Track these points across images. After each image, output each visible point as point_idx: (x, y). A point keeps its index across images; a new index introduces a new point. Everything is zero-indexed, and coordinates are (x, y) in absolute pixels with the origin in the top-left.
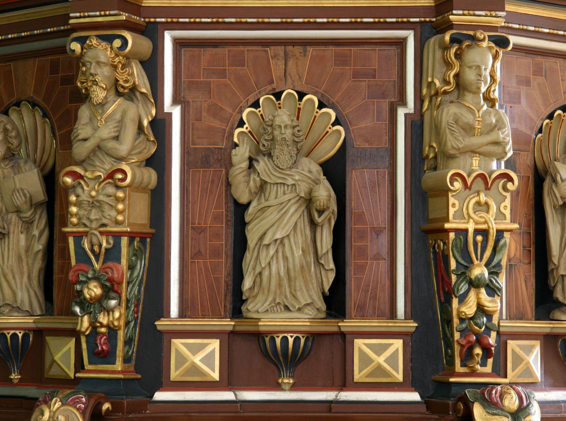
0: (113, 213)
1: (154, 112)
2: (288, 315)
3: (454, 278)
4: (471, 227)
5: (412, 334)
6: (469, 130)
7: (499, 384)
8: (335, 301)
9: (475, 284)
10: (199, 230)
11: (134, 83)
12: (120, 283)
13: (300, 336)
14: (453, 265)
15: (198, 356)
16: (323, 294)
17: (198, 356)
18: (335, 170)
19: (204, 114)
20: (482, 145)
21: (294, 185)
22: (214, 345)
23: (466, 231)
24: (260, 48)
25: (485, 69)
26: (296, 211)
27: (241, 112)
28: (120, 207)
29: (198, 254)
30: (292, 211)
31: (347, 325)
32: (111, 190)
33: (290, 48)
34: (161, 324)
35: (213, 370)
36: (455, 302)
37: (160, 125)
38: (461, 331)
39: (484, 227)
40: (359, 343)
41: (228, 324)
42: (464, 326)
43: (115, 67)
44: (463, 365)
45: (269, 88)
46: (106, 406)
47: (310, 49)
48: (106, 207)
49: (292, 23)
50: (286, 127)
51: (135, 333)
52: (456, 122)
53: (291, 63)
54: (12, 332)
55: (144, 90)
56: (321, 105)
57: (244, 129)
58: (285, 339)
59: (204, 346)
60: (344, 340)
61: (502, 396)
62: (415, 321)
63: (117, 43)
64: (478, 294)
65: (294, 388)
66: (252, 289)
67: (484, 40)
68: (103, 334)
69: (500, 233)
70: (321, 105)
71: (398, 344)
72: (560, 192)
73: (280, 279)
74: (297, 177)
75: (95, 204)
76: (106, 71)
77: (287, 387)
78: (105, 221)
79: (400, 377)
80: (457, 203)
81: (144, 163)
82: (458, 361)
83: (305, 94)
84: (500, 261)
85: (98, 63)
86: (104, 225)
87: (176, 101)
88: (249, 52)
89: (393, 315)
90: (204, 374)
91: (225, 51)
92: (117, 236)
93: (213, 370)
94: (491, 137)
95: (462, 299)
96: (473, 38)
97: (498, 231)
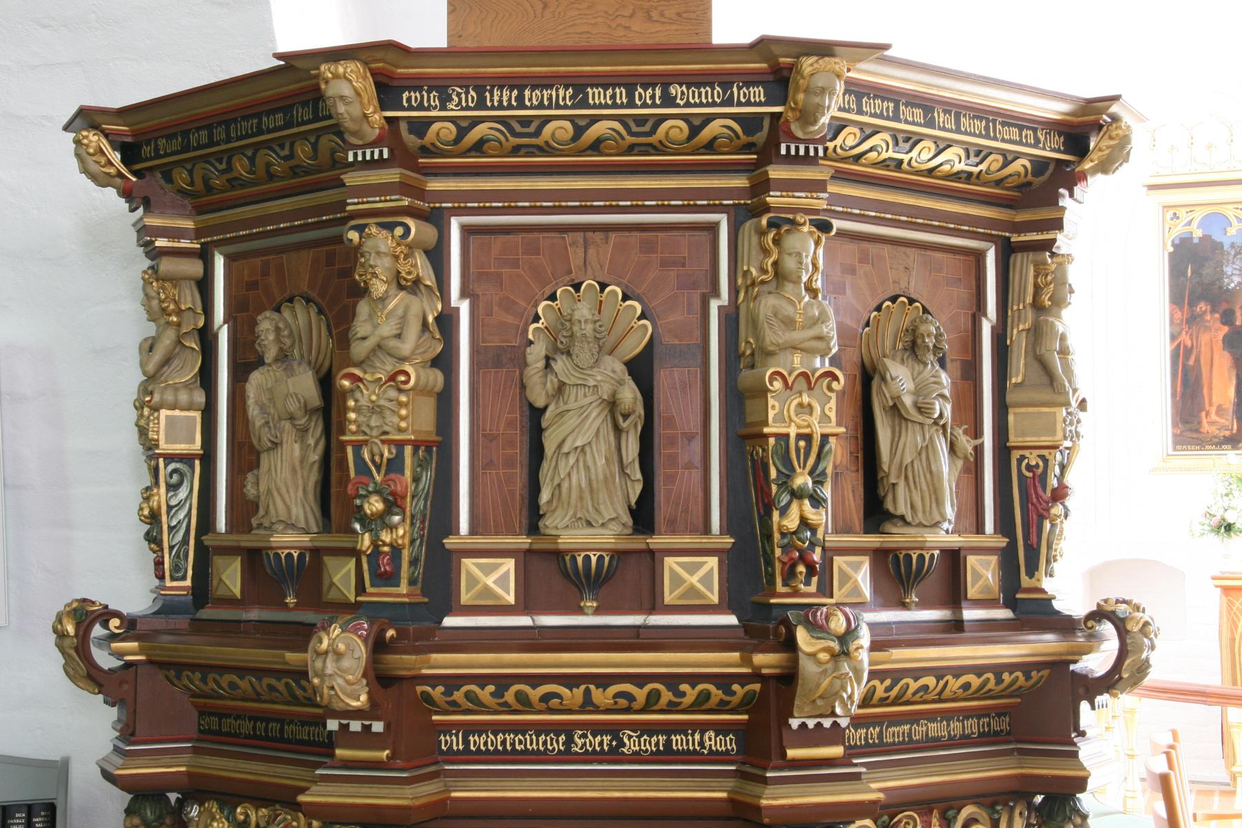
0: (396, 419)
1: (440, 307)
2: (590, 531)
3: (774, 488)
4: (793, 431)
5: (1002, 549)
6: (789, 323)
8: (643, 516)
9: (797, 495)
10: (491, 438)
12: (404, 497)
14: (773, 473)
15: (492, 577)
17: (492, 577)
18: (641, 369)
19: (495, 308)
21: (595, 386)
23: (787, 435)
26: (599, 415)
27: (536, 306)
28: (403, 412)
29: (489, 464)
31: (656, 541)
32: (392, 394)
33: (590, 234)
34: (450, 542)
35: (712, 593)
37: (447, 321)
39: (807, 431)
40: (670, 562)
41: (523, 541)
42: (786, 541)
43: (396, 258)
44: (785, 584)
45: (568, 278)
46: (391, 633)
48: (388, 413)
49: (618, 206)
50: (586, 321)
53: (591, 251)
55: (428, 283)
56: (626, 297)
57: (539, 325)
58: (587, 558)
59: (497, 566)
60: (653, 558)
61: (827, 619)
63: (399, 231)
64: (800, 506)
65: (598, 611)
66: (550, 502)
67: (804, 224)
68: (386, 553)
69: (825, 437)
70: (626, 297)
71: (712, 562)
74: (599, 378)
75: (376, 409)
76: (387, 261)
78: (386, 428)
80: (777, 404)
82: (779, 581)
83: (581, 283)
87: (464, 294)
89: (707, 530)
90: (497, 597)
92: (400, 445)
93: (712, 593)
95: (784, 511)
96: (793, 222)
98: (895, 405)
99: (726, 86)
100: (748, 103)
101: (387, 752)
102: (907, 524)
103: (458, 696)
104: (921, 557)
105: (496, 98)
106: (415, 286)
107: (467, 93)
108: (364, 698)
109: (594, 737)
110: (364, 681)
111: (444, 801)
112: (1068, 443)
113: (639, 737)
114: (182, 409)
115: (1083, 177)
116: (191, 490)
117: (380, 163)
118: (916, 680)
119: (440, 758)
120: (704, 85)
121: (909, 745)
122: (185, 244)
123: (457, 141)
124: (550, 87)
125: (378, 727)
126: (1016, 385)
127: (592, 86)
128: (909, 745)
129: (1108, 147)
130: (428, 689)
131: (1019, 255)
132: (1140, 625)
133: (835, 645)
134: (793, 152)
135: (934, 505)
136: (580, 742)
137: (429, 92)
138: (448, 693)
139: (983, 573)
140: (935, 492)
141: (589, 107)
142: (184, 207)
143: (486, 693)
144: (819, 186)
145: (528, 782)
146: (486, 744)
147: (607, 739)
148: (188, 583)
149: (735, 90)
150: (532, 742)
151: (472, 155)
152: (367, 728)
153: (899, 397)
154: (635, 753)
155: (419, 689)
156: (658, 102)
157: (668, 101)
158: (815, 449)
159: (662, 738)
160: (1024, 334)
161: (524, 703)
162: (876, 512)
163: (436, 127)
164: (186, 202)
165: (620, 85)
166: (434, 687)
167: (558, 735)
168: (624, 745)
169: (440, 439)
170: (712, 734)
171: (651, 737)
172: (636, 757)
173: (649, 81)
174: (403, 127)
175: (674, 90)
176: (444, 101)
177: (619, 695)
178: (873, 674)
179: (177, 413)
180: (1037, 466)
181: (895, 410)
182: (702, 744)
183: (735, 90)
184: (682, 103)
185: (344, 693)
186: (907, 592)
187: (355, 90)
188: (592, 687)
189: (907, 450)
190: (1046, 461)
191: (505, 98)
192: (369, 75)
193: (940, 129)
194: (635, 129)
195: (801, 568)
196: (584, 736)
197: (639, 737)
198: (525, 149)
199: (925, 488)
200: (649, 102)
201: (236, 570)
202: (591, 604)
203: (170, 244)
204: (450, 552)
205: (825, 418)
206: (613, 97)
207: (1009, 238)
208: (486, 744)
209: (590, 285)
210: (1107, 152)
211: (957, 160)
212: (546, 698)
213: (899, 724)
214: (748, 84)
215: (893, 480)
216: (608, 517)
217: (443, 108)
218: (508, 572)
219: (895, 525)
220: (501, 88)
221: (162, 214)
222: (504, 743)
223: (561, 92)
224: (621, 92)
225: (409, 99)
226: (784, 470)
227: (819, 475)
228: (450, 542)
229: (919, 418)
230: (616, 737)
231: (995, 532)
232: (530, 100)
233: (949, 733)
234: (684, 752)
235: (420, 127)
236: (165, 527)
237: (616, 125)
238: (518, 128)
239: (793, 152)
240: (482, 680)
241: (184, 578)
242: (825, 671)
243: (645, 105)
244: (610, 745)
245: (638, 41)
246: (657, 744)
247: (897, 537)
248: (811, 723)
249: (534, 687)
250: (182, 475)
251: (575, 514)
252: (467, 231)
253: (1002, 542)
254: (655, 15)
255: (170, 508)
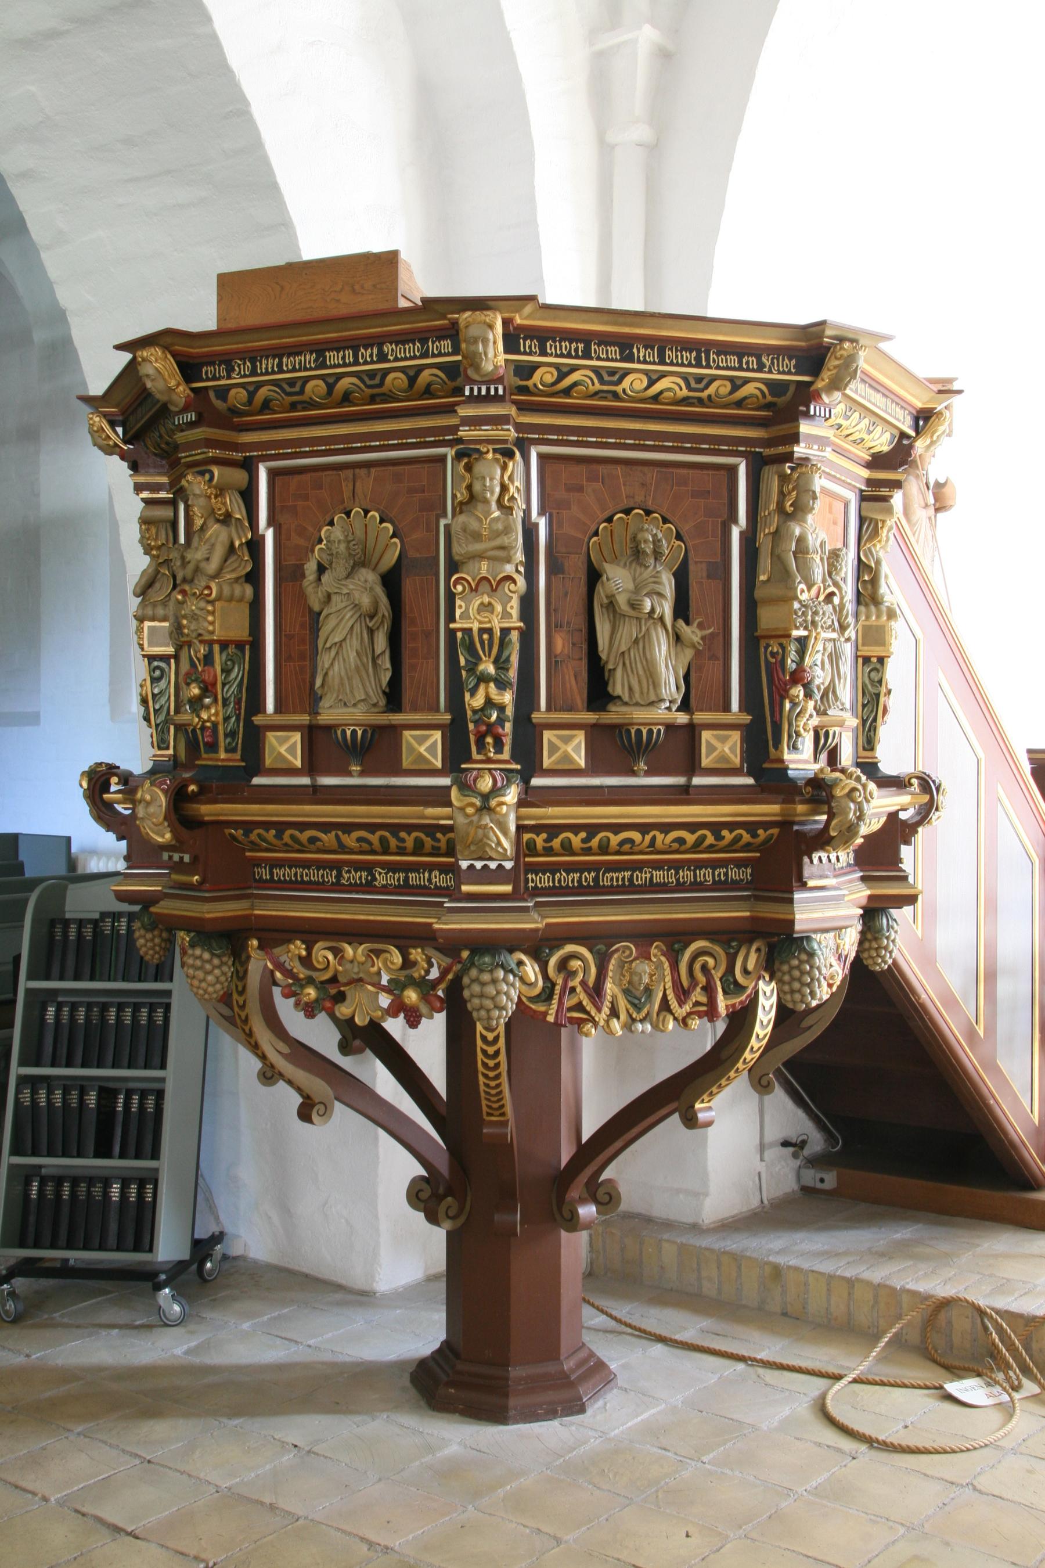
0: (206, 624)
1: (249, 537)
2: (345, 710)
3: (464, 673)
4: (475, 626)
5: (746, 726)
6: (477, 536)
7: (474, 769)
8: (393, 698)
9: (484, 679)
10: (290, 637)
11: (227, 510)
12: (214, 684)
13: (357, 729)
14: (462, 662)
15: (286, 747)
16: (384, 692)
17: (286, 747)
18: (391, 581)
19: (293, 534)
20: (486, 550)
21: (348, 594)
22: (297, 737)
23: (470, 630)
24: (335, 472)
25: (491, 479)
26: (352, 616)
27: (320, 531)
28: (210, 618)
29: (289, 658)
30: (347, 617)
31: (700, 717)
32: (202, 604)
33: (357, 471)
34: (258, 720)
35: (436, 759)
36: (467, 695)
37: (255, 546)
38: (476, 722)
39: (488, 626)
40: (407, 734)
41: (305, 719)
42: (477, 717)
43: (209, 497)
44: (478, 753)
45: (342, 507)
46: (192, 788)
47: (373, 470)
48: (201, 619)
49: (370, 446)
50: (339, 541)
51: (238, 726)
52: (465, 531)
53: (358, 484)
54: (636, 727)
55: (238, 516)
56: (382, 521)
57: (322, 546)
58: (354, 732)
59: (427, 737)
60: (395, 731)
61: (475, 781)
62: (749, 714)
63: (207, 476)
64: (487, 688)
65: (362, 774)
66: (323, 685)
67: (488, 452)
68: (209, 728)
69: (505, 631)
70: (382, 521)
71: (437, 735)
72: (604, 591)
73: (341, 679)
74: (351, 587)
75: (194, 617)
76: (202, 501)
77: (642, 773)
78: (200, 631)
79: (439, 764)
80: (463, 604)
81: (243, 579)
82: (474, 748)
83: (351, 511)
84: (509, 656)
85: (194, 495)
86: (200, 635)
87: (270, 522)
88: (326, 477)
89: (727, 708)
90: (291, 763)
91: (307, 477)
92: (210, 643)
93: (436, 759)
94: (498, 542)
95: (473, 692)
96: (478, 451)
97: (502, 630)
98: (611, 602)
99: (424, 341)
100: (440, 355)
101: (196, 877)
102: (626, 704)
103: (556, 843)
104: (650, 732)
105: (264, 366)
106: (226, 519)
107: (244, 364)
108: (168, 836)
109: (356, 872)
110: (166, 824)
111: (247, 917)
112: (801, 633)
113: (386, 874)
114: (160, 621)
115: (816, 396)
116: (169, 682)
117: (192, 425)
118: (731, 832)
119: (254, 885)
120: (408, 342)
121: (631, 887)
122: (163, 495)
123: (250, 401)
124: (299, 353)
125: (187, 858)
126: (764, 582)
127: (329, 350)
128: (631, 887)
129: (835, 367)
130: (533, 836)
131: (767, 467)
132: (846, 790)
133: (478, 802)
134: (492, 392)
135: (651, 687)
136: (346, 876)
137: (219, 366)
138: (246, 834)
139: (722, 747)
140: (651, 676)
141: (326, 367)
142: (162, 466)
143: (576, 840)
144: (503, 420)
145: (567, 910)
146: (284, 875)
147: (364, 874)
148: (171, 752)
149: (430, 344)
150: (314, 875)
151: (258, 413)
152: (181, 858)
153: (613, 596)
154: (384, 886)
155: (227, 831)
156: (580, 354)
157: (382, 358)
158: (496, 641)
159: (402, 875)
160: (771, 537)
161: (604, 849)
162: (599, 694)
163: (233, 392)
164: (164, 462)
165: (348, 348)
166: (267, 831)
167: (332, 871)
168: (376, 879)
169: (251, 639)
170: (438, 873)
171: (394, 873)
172: (385, 890)
173: (368, 342)
174: (212, 394)
175: (387, 348)
176: (230, 370)
177: (359, 840)
178: (520, 829)
179: (156, 624)
180: (778, 652)
181: (611, 605)
182: (430, 880)
183: (430, 344)
184: (391, 358)
185: (153, 832)
186: (636, 761)
187: (156, 368)
188: (340, 833)
189: (623, 641)
190: (783, 648)
191: (270, 366)
192: (169, 356)
193: (639, 362)
194: (369, 382)
195: (489, 740)
196: (349, 872)
197: (386, 874)
198: (297, 407)
199: (641, 672)
200: (368, 359)
201: (580, 742)
202: (355, 768)
203: (151, 496)
204: (258, 727)
205: (506, 615)
206: (344, 358)
207: (761, 453)
208: (284, 875)
209: (357, 512)
210: (834, 372)
211: (677, 388)
212: (313, 840)
213: (619, 870)
214: (440, 338)
215: (610, 666)
216: (358, 698)
217: (229, 377)
218: (296, 742)
219: (615, 704)
220: (267, 358)
221: (147, 474)
222: (296, 874)
223: (308, 357)
224: (349, 353)
225: (747, 363)
226: (470, 659)
227: (504, 662)
228: (258, 720)
229: (632, 613)
230: (371, 873)
231: (740, 711)
232: (287, 365)
233: (678, 880)
234: (420, 887)
235: (223, 393)
236: (152, 710)
237: (354, 380)
238: (288, 389)
239: (476, 393)
240: (575, 828)
241: (168, 748)
242: (471, 822)
243: (366, 363)
244: (366, 879)
245: (343, 311)
246: (399, 880)
247: (614, 714)
248: (479, 865)
249: (301, 832)
250: (162, 670)
251: (338, 696)
252: (273, 474)
253: (747, 718)
254: (357, 287)
255: (154, 695)
